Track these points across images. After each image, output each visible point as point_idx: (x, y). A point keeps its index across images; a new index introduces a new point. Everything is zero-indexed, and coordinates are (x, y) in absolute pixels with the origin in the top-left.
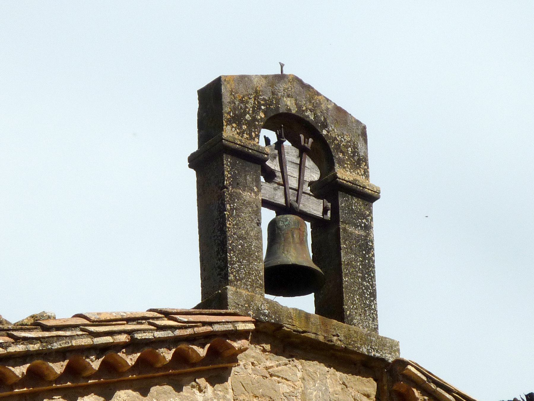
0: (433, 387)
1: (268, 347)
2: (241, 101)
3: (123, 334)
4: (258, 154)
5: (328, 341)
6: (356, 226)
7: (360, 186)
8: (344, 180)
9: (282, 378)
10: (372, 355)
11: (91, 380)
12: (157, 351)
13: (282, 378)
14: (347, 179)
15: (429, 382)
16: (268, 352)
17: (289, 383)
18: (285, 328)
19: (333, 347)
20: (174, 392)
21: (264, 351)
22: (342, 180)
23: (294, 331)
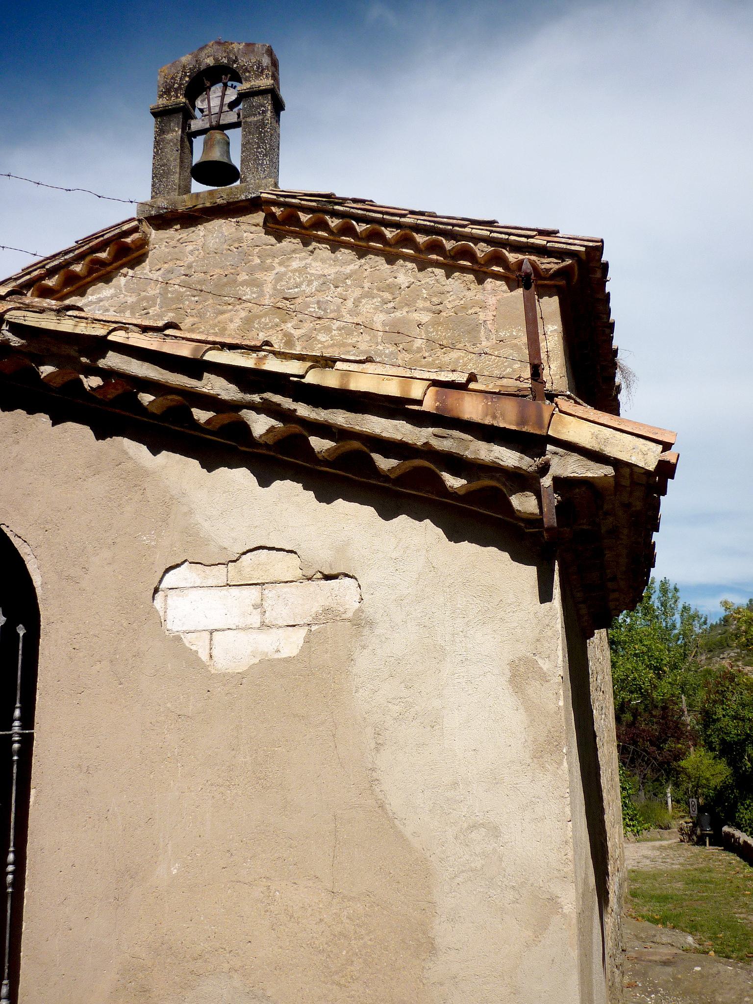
0: (282, 200)
1: (178, 227)
2: (172, 78)
3: (106, 261)
4: (177, 106)
5: (214, 204)
6: (255, 115)
7: (256, 88)
8: (248, 89)
9: (189, 242)
10: (249, 197)
11: (497, 266)
12: (70, 269)
13: (189, 242)
14: (245, 88)
15: (279, 198)
16: (180, 229)
17: (193, 243)
18: (179, 210)
19: (219, 206)
20: (106, 285)
21: (176, 230)
22: (242, 90)
23: (186, 209)
